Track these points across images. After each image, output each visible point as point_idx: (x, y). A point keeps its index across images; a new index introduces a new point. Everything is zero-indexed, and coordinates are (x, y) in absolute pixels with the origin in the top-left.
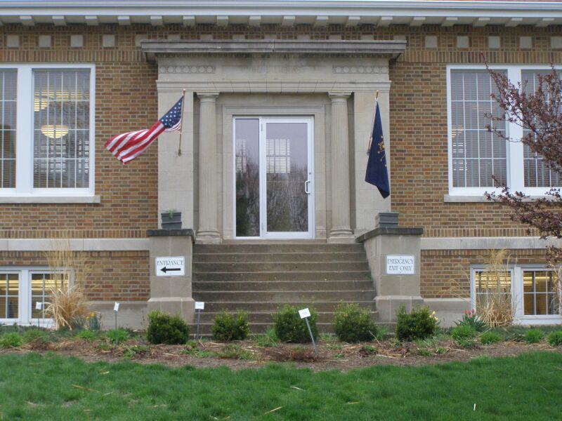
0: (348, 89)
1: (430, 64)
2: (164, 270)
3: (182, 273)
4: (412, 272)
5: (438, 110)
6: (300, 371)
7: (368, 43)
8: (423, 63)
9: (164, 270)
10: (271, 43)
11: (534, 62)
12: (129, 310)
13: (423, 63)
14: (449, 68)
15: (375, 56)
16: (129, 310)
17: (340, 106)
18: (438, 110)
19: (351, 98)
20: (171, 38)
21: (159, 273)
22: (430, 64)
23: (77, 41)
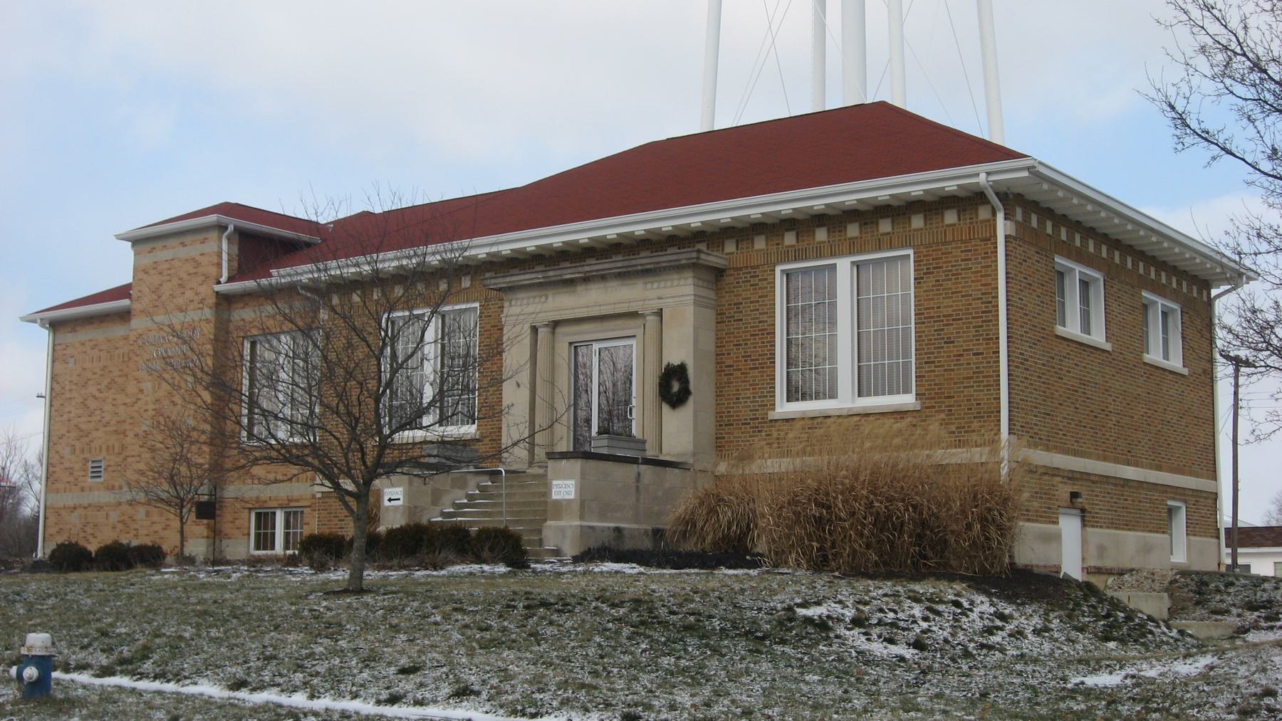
0: (656, 305)
1: (758, 267)
2: (390, 500)
3: (400, 503)
4: (572, 497)
5: (765, 318)
6: (782, 586)
7: (671, 255)
8: (752, 267)
9: (390, 500)
10: (593, 266)
11: (861, 252)
12: (93, 547)
13: (752, 267)
14: (778, 269)
15: (679, 268)
16: (93, 547)
17: (651, 320)
18: (765, 318)
19: (660, 313)
20: (589, 261)
21: (387, 503)
22: (758, 267)
23: (885, 226)
